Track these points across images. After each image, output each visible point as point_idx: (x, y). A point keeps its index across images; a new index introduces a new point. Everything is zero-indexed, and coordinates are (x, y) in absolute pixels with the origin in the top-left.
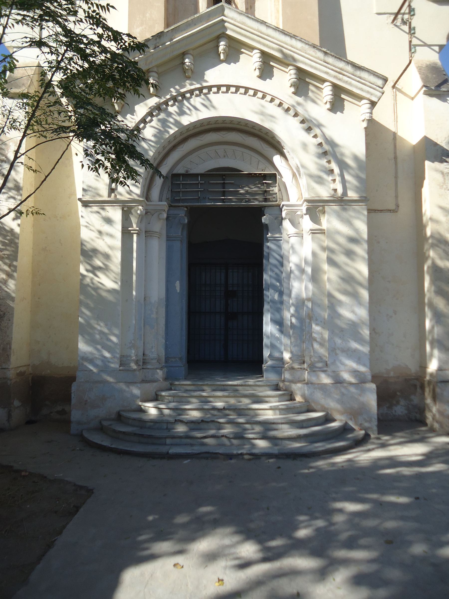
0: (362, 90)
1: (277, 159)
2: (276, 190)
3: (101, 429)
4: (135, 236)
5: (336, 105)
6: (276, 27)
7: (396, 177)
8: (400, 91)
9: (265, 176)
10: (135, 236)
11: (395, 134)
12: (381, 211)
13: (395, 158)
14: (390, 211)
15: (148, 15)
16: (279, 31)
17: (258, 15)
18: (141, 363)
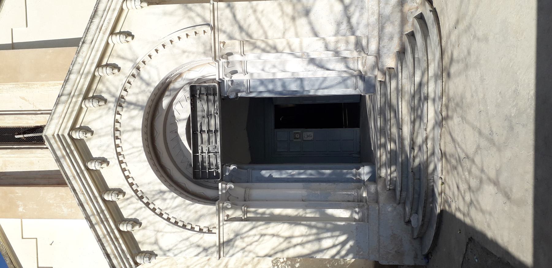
3: (421, 238)
15: (51, 202)
18: (361, 204)
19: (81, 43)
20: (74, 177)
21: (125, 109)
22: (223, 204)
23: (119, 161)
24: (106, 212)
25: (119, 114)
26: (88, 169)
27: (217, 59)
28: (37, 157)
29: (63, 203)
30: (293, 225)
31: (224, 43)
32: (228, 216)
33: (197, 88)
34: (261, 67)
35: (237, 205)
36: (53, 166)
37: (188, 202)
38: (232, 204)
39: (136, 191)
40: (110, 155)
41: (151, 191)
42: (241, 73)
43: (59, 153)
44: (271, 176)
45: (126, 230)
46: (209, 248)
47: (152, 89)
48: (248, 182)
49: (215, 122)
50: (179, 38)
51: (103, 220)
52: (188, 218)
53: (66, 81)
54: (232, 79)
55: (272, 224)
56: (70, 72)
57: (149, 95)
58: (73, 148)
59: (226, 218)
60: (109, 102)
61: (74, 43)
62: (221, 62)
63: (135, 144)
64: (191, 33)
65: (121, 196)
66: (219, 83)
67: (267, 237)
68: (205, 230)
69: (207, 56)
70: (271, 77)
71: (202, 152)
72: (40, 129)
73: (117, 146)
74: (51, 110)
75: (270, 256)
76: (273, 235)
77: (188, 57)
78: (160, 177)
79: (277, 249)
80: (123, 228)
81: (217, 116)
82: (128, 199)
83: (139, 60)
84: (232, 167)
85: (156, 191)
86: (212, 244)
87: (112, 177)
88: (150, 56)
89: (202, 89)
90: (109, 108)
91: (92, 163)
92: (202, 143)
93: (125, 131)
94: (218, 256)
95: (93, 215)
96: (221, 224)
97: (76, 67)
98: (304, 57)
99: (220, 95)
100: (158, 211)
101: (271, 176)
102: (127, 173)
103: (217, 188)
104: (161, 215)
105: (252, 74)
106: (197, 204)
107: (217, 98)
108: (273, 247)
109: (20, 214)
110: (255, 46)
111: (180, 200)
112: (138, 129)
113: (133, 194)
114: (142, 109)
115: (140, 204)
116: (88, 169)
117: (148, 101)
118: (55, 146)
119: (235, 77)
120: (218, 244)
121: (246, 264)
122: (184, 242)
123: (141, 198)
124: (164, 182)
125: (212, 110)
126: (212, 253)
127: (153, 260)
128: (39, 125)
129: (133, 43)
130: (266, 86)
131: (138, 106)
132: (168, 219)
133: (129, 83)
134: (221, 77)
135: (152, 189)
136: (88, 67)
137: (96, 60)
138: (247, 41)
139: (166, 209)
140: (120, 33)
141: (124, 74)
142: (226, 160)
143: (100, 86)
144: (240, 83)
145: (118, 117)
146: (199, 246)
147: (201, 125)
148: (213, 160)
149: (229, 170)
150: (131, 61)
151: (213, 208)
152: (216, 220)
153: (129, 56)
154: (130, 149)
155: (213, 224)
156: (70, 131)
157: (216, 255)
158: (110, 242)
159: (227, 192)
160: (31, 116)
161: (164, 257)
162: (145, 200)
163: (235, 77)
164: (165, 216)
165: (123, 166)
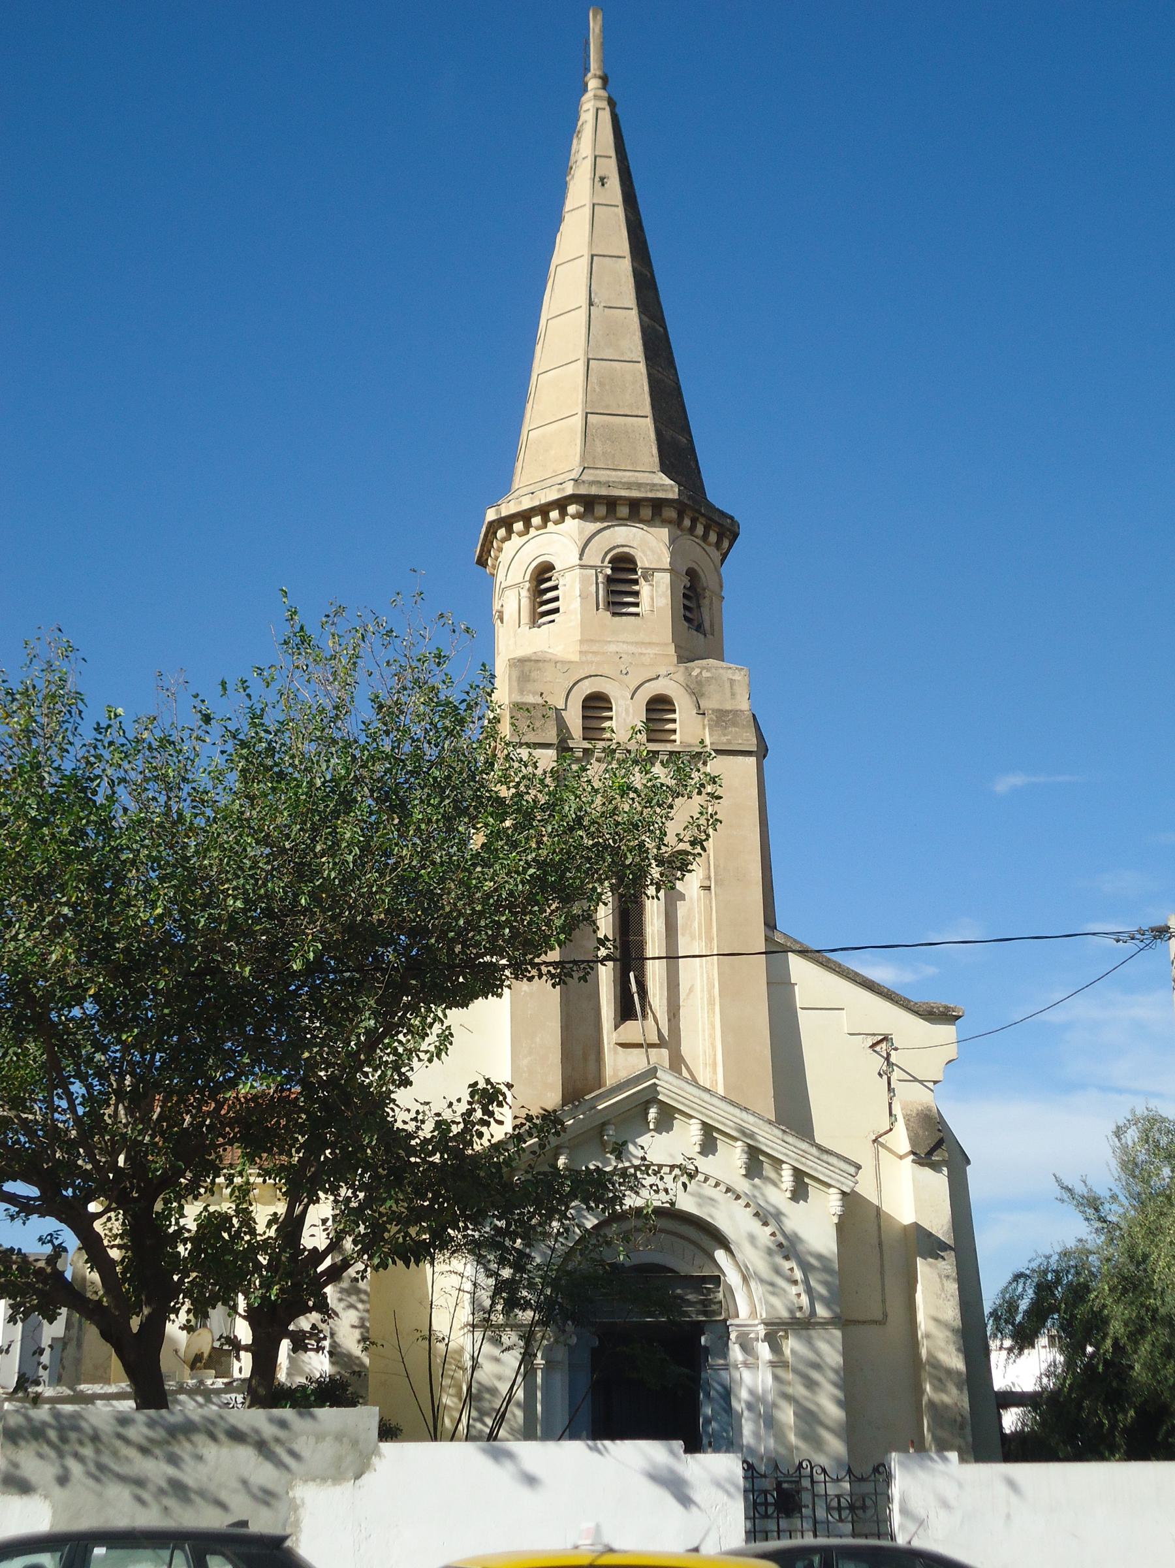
0: (830, 1177)
1: (720, 1255)
2: (720, 1296)
4: (539, 1373)
5: (799, 1193)
7: (882, 1273)
8: (883, 1146)
9: (704, 1279)
10: (539, 1373)
11: (878, 1209)
12: (864, 1322)
13: (880, 1244)
14: (875, 1322)
15: (538, 1040)
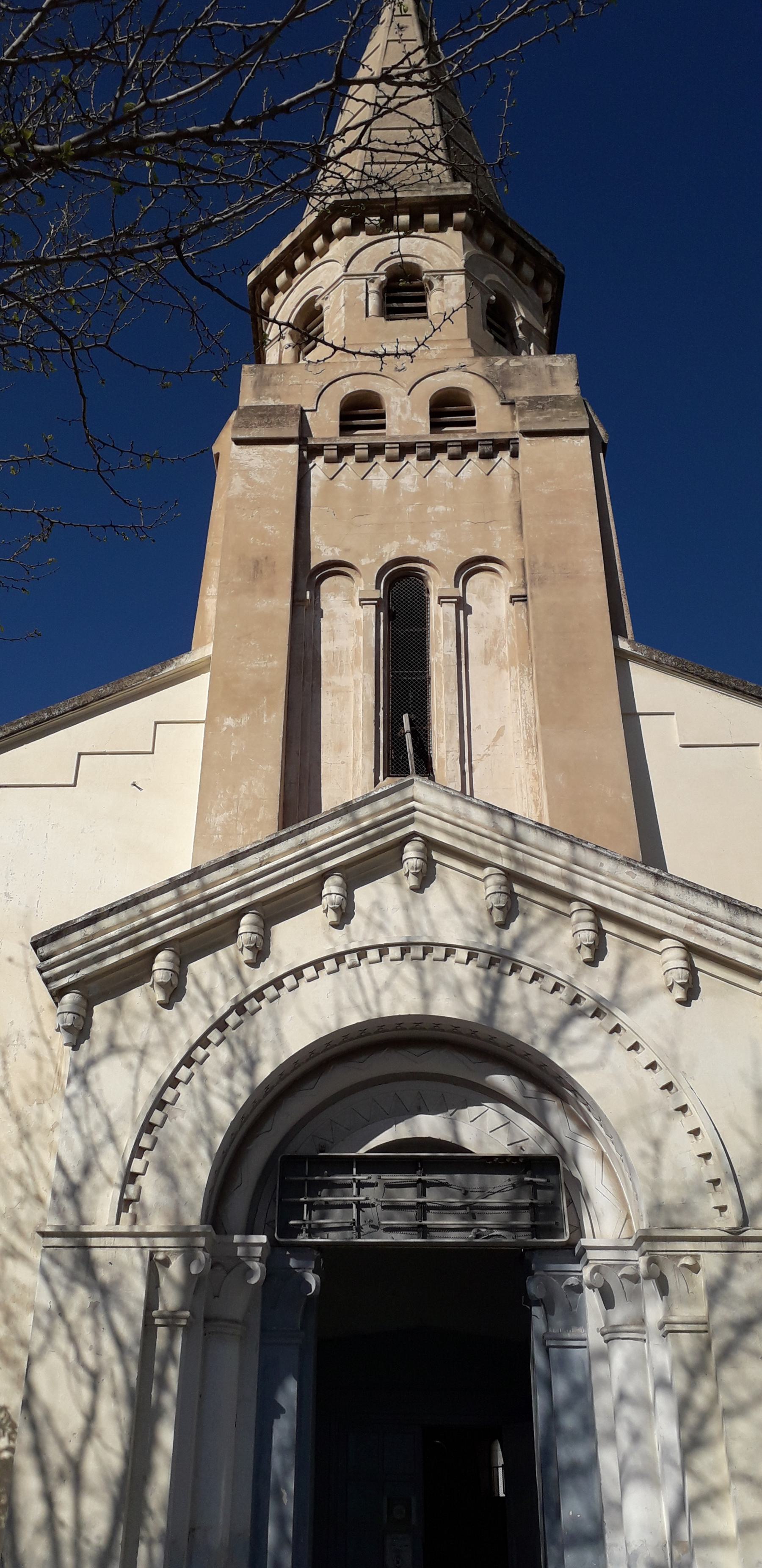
6: (536, 823)
15: (243, 788)
16: (542, 830)
17: (674, 866)
19: (656, 871)
20: (306, 844)
21: (481, 972)
22: (204, 1249)
23: (343, 954)
24: (208, 918)
25: (469, 959)
26: (324, 876)
27: (645, 1246)
28: (355, 760)
29: (237, 815)
30: (115, 1489)
31: (695, 1269)
32: (166, 1263)
33: (553, 1179)
34: (631, 1389)
35: (195, 1293)
36: (331, 795)
37: (219, 1139)
38: (200, 1278)
39: (259, 995)
40: (359, 932)
41: (256, 1035)
42: (606, 1321)
43: (363, 812)
44: (278, 1411)
45: (155, 966)
46: (77, 1205)
47: (541, 1046)
48: (263, 1330)
49: (450, 1230)
50: (696, 1132)
51: (189, 911)
52: (172, 1140)
53: (551, 832)
54: (586, 1289)
55: (125, 1415)
56: (573, 841)
57: (525, 1038)
58: (378, 843)
59: (160, 1256)
60: (499, 934)
61: (651, 854)
62: (634, 1255)
63: (386, 999)
64: (712, 1169)
65: (247, 955)
66: (570, 1246)
67: (86, 1394)
68: (131, 1190)
69: (650, 1213)
70: (601, 1423)
71: (361, 1185)
72: (425, 767)
73: (383, 950)
74: (472, 795)
75: (26, 1405)
76: (91, 1417)
77: (643, 1155)
78: (295, 1061)
79: (45, 1430)
80: (162, 961)
81: (471, 1235)
82: (239, 972)
83: (621, 1017)
84: (313, 1280)
85: (257, 1049)
86: (86, 1212)
87: (301, 937)
88: (635, 1047)
89: (550, 1193)
90: (481, 934)
91: (340, 886)
92: (389, 1186)
93: (421, 974)
94: (48, 1230)
95: (205, 887)
96: (144, 1241)
97: (590, 858)
98: (676, 1553)
99: (533, 1249)
100: (200, 1052)
101: (278, 1411)
102: (309, 972)
103: (250, 1230)
104: (188, 1061)
105: (604, 1356)
106: (209, 1167)
107: (524, 1237)
108: (55, 1415)
109: (218, 720)
110: (695, 1372)
111: (226, 1114)
112: (426, 1006)
113: (253, 988)
114: (482, 1013)
115: (222, 1005)
116: (324, 876)
117: (508, 1036)
118: (383, 803)
119: (592, 1300)
120: (86, 1229)
121: (9, 1317)
122: (104, 1128)
123: (239, 1008)
124: (280, 1072)
125: (487, 1221)
126: (59, 1212)
127: (60, 1039)
128: (435, 765)
129: (666, 1004)
130: (569, 1405)
131: (493, 1010)
132: (173, 1082)
133: (556, 988)
134: (590, 1254)
135: (264, 1037)
136: (590, 883)
137: (610, 906)
138: (709, 1345)
139: (204, 1078)
140: (693, 971)
141: (577, 975)
142: (335, 1260)
143: (539, 912)
144: (575, 1317)
145: (463, 955)
146: (87, 1170)
147: (440, 1184)
148: (336, 1218)
149: (305, 1269)
150: (616, 995)
151: (193, 1218)
152: (157, 1224)
153: (630, 988)
154: (374, 982)
155: (145, 1216)
156: (423, 837)
157: (52, 1223)
158: (126, 928)
159: (238, 1261)
160: (458, 749)
161: (66, 1070)
162: (232, 1019)
163: (592, 1300)
164: (183, 1073)
165: (330, 965)
